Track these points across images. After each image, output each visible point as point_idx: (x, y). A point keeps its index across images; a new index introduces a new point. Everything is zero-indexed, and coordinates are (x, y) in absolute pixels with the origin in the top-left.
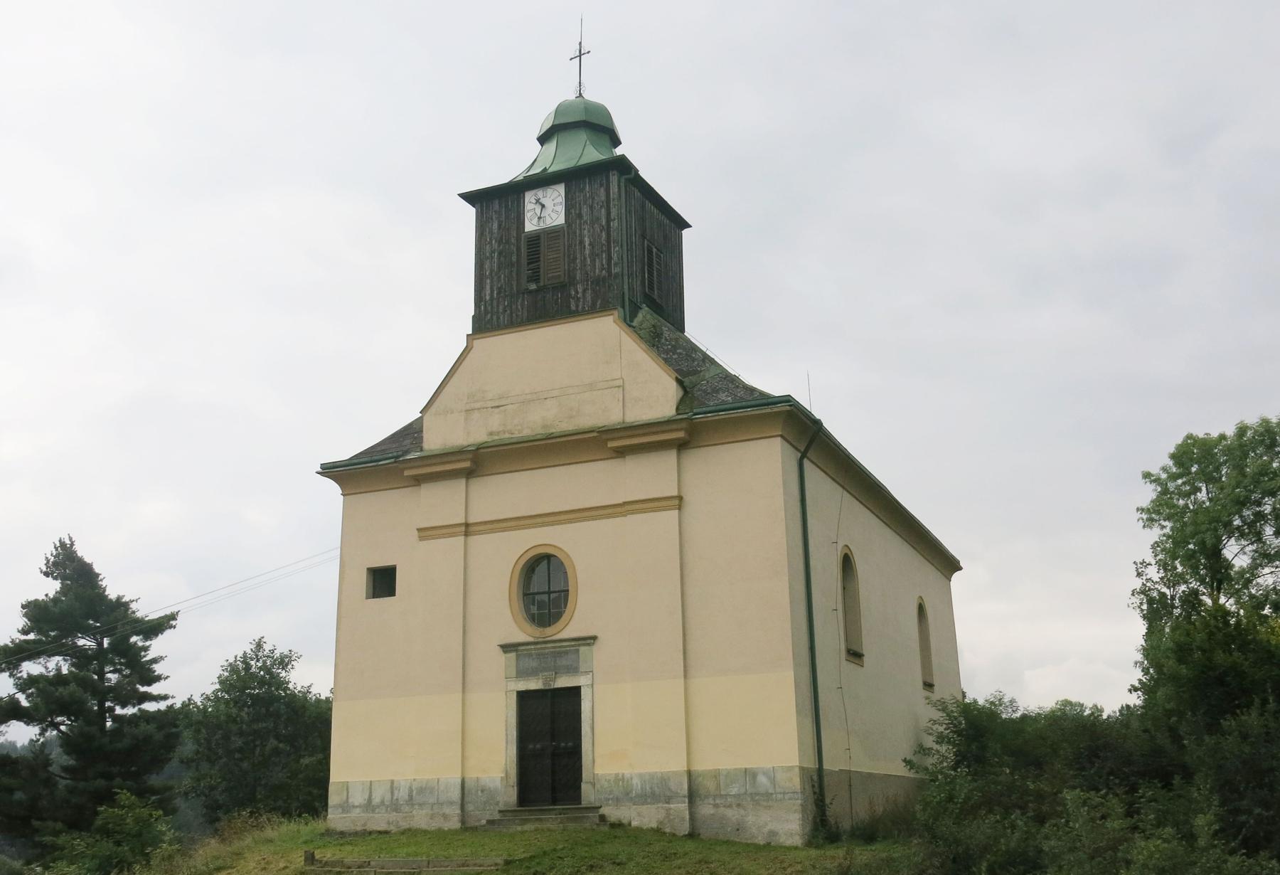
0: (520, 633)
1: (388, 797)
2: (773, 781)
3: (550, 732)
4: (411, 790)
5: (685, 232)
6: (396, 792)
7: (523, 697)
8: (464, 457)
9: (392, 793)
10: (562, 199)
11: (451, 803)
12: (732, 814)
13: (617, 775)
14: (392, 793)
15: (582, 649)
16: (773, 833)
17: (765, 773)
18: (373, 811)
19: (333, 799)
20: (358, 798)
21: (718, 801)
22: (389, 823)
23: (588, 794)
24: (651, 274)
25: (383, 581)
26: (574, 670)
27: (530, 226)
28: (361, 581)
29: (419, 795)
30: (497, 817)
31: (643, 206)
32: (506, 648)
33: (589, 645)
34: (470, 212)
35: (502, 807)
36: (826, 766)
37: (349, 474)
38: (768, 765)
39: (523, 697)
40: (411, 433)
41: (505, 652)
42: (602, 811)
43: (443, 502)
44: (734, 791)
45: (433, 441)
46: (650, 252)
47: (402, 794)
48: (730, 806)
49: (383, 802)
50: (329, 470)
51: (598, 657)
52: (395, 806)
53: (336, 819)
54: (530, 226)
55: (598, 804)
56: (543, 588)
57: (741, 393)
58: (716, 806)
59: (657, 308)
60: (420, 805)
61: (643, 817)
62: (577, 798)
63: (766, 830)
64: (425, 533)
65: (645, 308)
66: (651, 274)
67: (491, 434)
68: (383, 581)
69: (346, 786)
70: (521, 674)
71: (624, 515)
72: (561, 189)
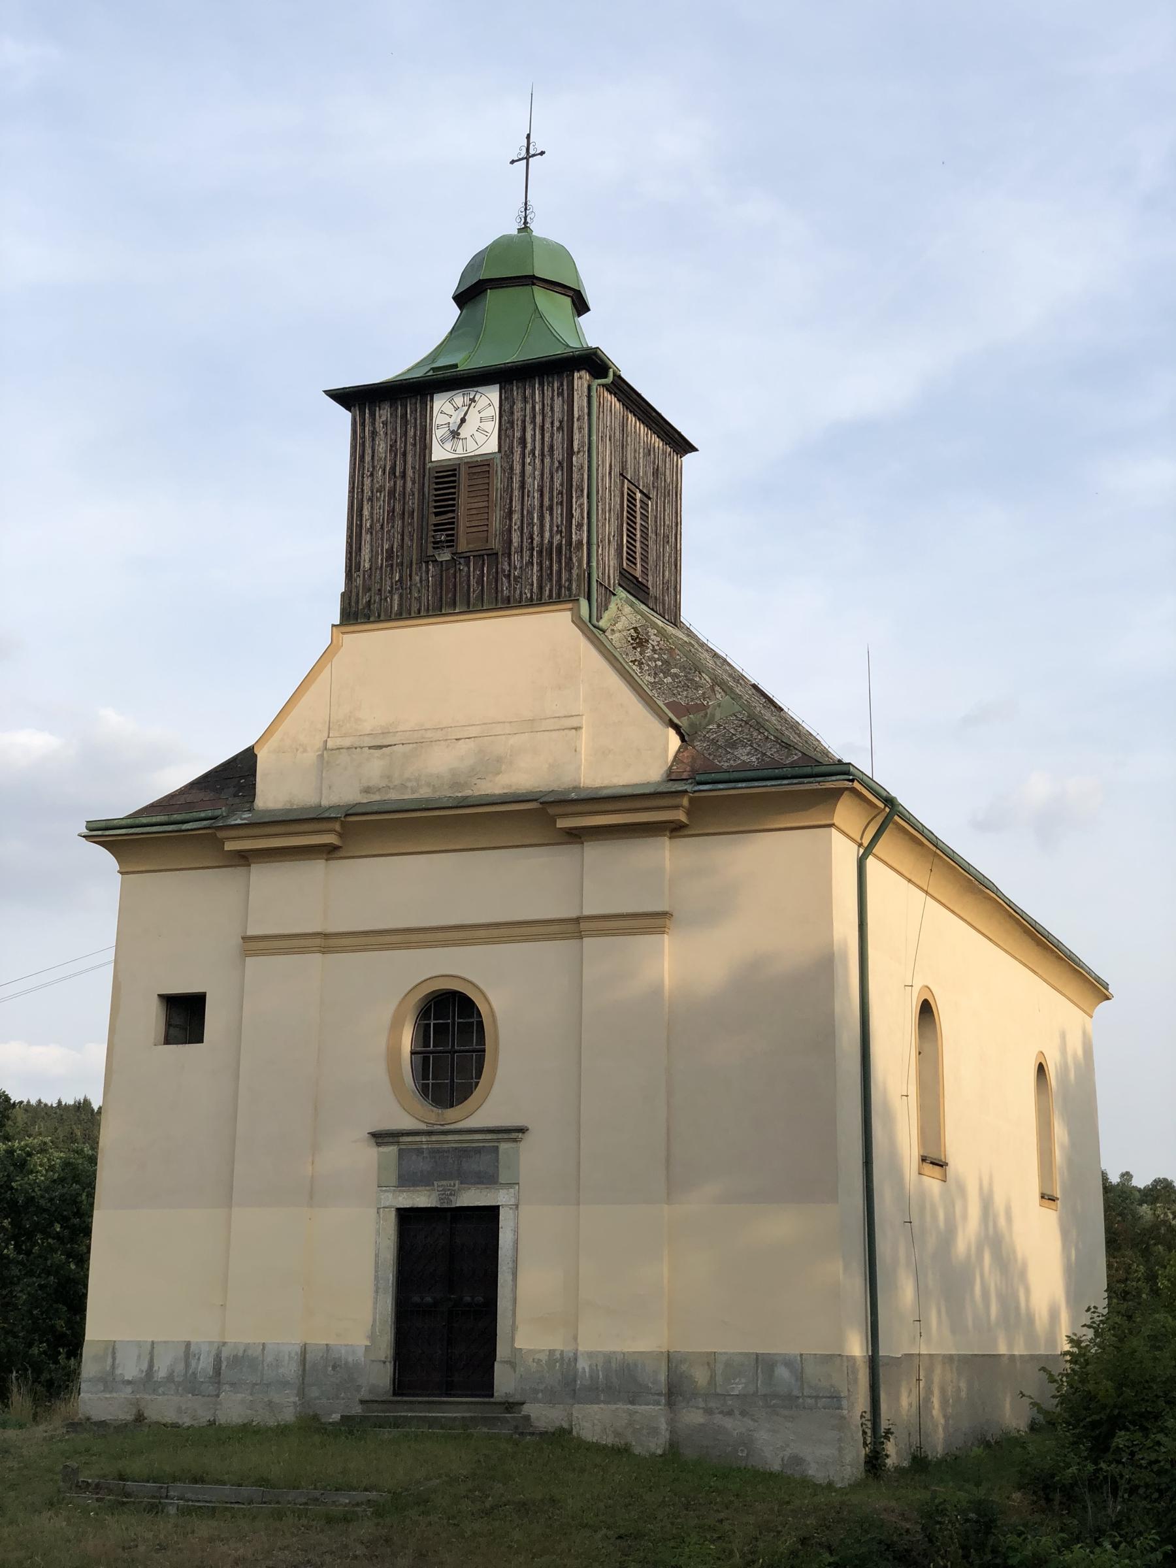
0: (405, 1114)
1: (180, 1367)
2: (800, 1376)
3: (446, 1272)
4: (218, 1359)
5: (688, 460)
6: (193, 1363)
7: (406, 1217)
8: (329, 826)
9: (187, 1365)
10: (494, 411)
11: (285, 1384)
12: (733, 1426)
13: (552, 1352)
14: (187, 1365)
15: (503, 1146)
16: (797, 1460)
17: (788, 1363)
18: (155, 1391)
19: (90, 1366)
20: (130, 1369)
21: (712, 1404)
22: (179, 1410)
23: (505, 1382)
24: (631, 536)
25: (185, 1016)
26: (489, 1179)
27: (440, 453)
28: (152, 1017)
29: (228, 1368)
30: (357, 1410)
31: (623, 425)
32: (380, 1138)
33: (515, 1140)
34: (343, 418)
35: (364, 1394)
36: (882, 1352)
37: (136, 839)
38: (791, 1349)
39: (406, 1217)
40: (236, 776)
41: (378, 1144)
42: (527, 1409)
43: (289, 895)
44: (738, 1389)
45: (273, 792)
46: (632, 498)
47: (205, 1364)
48: (730, 1413)
49: (170, 1378)
50: (102, 833)
51: (530, 1160)
52: (190, 1384)
53: (93, 1400)
54: (440, 453)
55: (518, 1398)
56: (450, 1036)
57: (772, 751)
58: (709, 1411)
59: (638, 589)
60: (232, 1384)
61: (594, 1422)
62: (486, 1385)
63: (788, 1452)
64: (255, 945)
65: (621, 593)
66: (631, 536)
67: (367, 790)
68: (185, 1016)
69: (112, 1348)
70: (406, 1180)
71: (408, 946)
72: (489, 398)
